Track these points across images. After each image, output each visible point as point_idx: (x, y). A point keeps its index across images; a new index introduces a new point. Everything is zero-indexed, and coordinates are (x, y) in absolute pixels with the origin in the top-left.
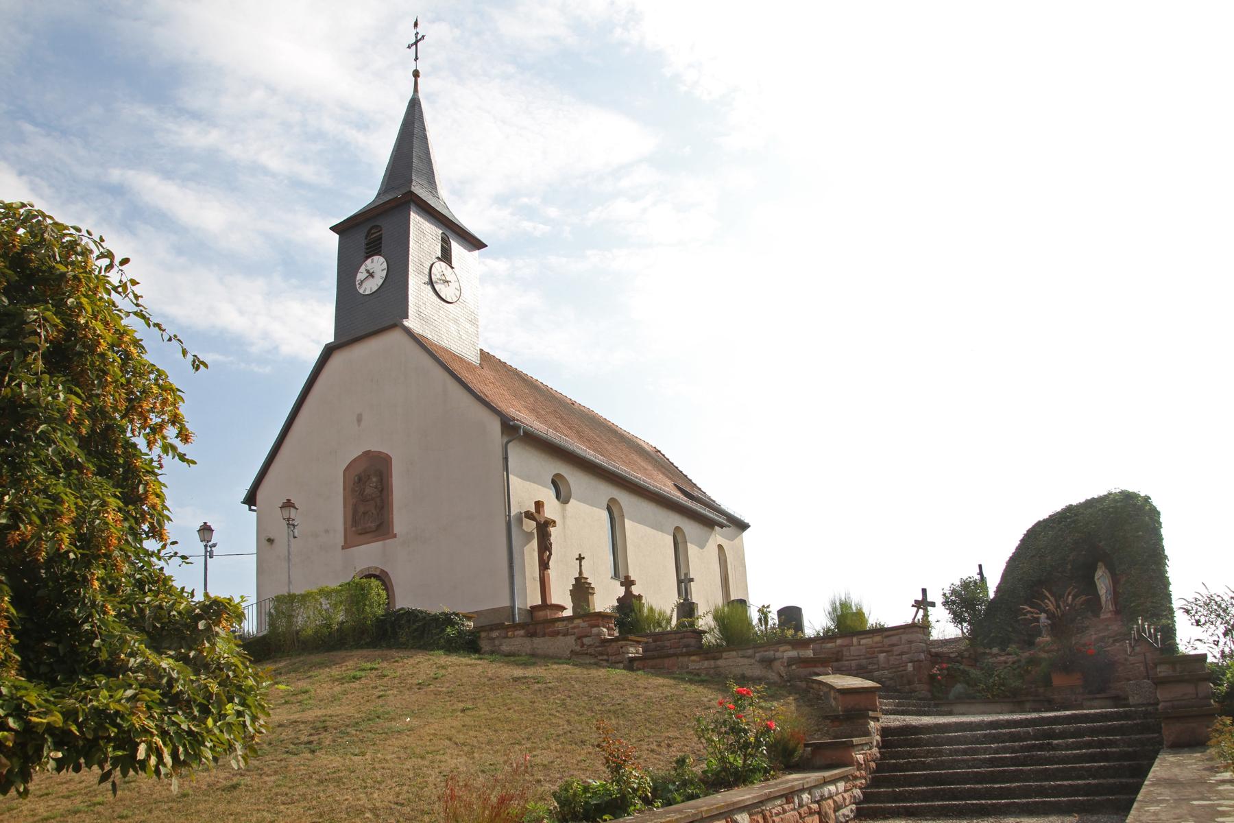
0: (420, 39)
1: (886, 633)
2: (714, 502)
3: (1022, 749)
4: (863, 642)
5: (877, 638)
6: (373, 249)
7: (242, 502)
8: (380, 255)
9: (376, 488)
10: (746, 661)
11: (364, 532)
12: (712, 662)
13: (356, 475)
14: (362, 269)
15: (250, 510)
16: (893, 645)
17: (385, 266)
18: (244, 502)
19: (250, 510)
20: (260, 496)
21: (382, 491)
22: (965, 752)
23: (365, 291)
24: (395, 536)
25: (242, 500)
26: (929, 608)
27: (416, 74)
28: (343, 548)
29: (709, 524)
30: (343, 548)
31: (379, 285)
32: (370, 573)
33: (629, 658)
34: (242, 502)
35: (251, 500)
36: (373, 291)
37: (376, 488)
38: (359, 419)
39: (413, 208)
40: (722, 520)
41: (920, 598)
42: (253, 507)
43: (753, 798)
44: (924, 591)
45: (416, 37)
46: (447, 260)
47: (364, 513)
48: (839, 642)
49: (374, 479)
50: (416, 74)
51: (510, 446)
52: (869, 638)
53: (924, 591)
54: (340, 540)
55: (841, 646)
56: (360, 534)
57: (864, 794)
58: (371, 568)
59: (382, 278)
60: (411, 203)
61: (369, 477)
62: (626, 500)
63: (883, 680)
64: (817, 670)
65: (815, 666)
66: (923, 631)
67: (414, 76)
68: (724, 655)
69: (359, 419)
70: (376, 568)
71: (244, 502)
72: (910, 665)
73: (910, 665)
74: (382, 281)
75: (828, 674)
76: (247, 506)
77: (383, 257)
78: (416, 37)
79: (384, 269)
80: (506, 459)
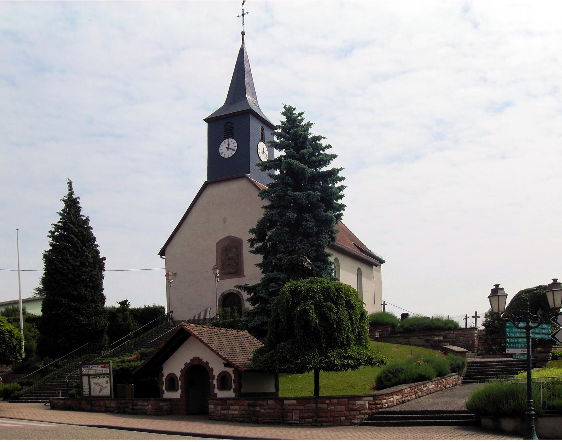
1: (463, 330)
2: (370, 251)
3: (504, 368)
4: (455, 332)
5: (460, 332)
6: (229, 134)
7: (158, 254)
8: (233, 138)
9: (235, 253)
10: (420, 340)
11: (228, 274)
12: (407, 340)
13: (223, 247)
15: (161, 257)
16: (466, 334)
18: (158, 254)
19: (161, 257)
20: (167, 252)
21: (237, 256)
22: (489, 368)
23: (225, 155)
24: (245, 276)
25: (158, 253)
26: (477, 319)
27: (243, 33)
32: (231, 292)
33: (376, 337)
34: (158, 254)
35: (162, 253)
36: (230, 156)
37: (235, 253)
38: (225, 220)
39: (250, 114)
41: (474, 315)
42: (162, 257)
43: (400, 386)
44: (476, 312)
45: (243, 12)
46: (263, 140)
47: (229, 265)
48: (446, 332)
49: (234, 250)
50: (243, 33)
53: (476, 312)
55: (447, 334)
56: (226, 274)
57: (463, 378)
58: (232, 290)
60: (250, 114)
64: (445, 344)
65: (444, 343)
67: (242, 34)
68: (413, 338)
69: (225, 220)
71: (158, 254)
72: (471, 341)
73: (471, 341)
74: (231, 155)
75: (448, 345)
76: (160, 256)
77: (234, 139)
78: (243, 12)
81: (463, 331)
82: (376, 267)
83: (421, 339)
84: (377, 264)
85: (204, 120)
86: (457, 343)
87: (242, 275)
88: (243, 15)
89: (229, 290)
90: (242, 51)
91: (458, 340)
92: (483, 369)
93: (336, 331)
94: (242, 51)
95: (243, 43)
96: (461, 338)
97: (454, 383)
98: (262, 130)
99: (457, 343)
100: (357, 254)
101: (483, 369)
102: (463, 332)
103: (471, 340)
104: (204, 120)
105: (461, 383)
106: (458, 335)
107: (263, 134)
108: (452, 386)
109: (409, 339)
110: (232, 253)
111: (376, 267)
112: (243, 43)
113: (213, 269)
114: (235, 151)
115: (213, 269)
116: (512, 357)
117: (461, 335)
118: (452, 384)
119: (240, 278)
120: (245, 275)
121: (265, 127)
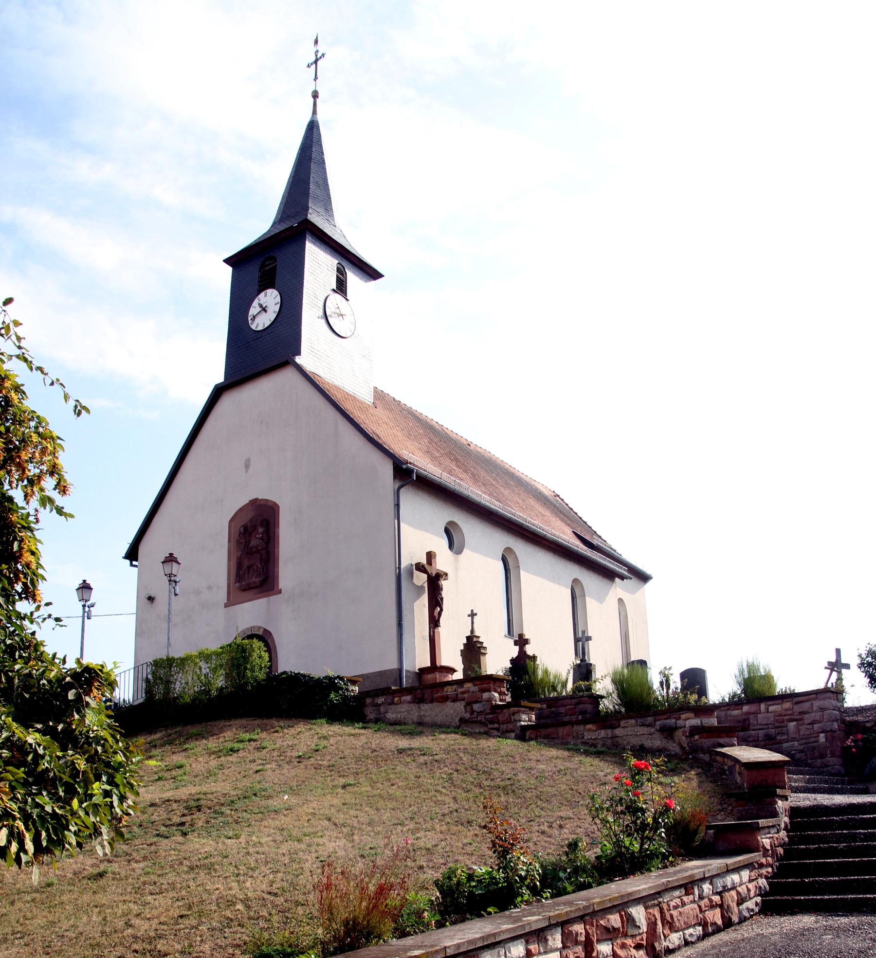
0: (320, 58)
4: (771, 708)
5: (787, 705)
6: (266, 283)
9: (262, 539)
10: (645, 730)
12: (609, 731)
13: (242, 526)
14: (255, 303)
15: (132, 565)
17: (278, 299)
27: (315, 95)
28: (226, 606)
29: (609, 575)
30: (226, 606)
31: (272, 320)
32: (253, 632)
35: (132, 554)
40: (623, 571)
44: (838, 651)
45: (316, 56)
46: (343, 292)
49: (260, 530)
50: (315, 95)
51: (402, 491)
52: (778, 704)
53: (838, 651)
54: (222, 595)
55: (748, 713)
57: (769, 884)
59: (275, 312)
61: (255, 528)
62: (523, 551)
63: (793, 752)
66: (837, 696)
70: (259, 628)
72: (822, 735)
73: (822, 735)
74: (275, 316)
75: (733, 745)
76: (128, 562)
77: (277, 290)
78: (316, 56)
79: (278, 303)
80: (397, 506)
81: (797, 703)
82: (623, 580)
83: (648, 726)
84: (626, 575)
85: (224, 261)
86: (780, 742)
87: (276, 590)
88: (316, 62)
89: (248, 629)
90: (312, 128)
91: (783, 734)
92: (854, 838)
93: (571, 737)
94: (312, 128)
95: (314, 112)
96: (792, 724)
97: (715, 916)
98: (341, 272)
99: (780, 742)
100: (576, 548)
101: (854, 838)
102: (796, 707)
103: (822, 732)
104: (224, 261)
105: (757, 910)
106: (780, 715)
107: (344, 280)
108: (705, 935)
109: (613, 727)
110: (256, 538)
111: (623, 580)
112: (314, 112)
113: (162, 563)
114: (812, 702)
115: (162, 563)
116: (655, 924)
117: (790, 715)
118: (704, 924)
119: (272, 598)
120: (281, 589)
121: (345, 263)
